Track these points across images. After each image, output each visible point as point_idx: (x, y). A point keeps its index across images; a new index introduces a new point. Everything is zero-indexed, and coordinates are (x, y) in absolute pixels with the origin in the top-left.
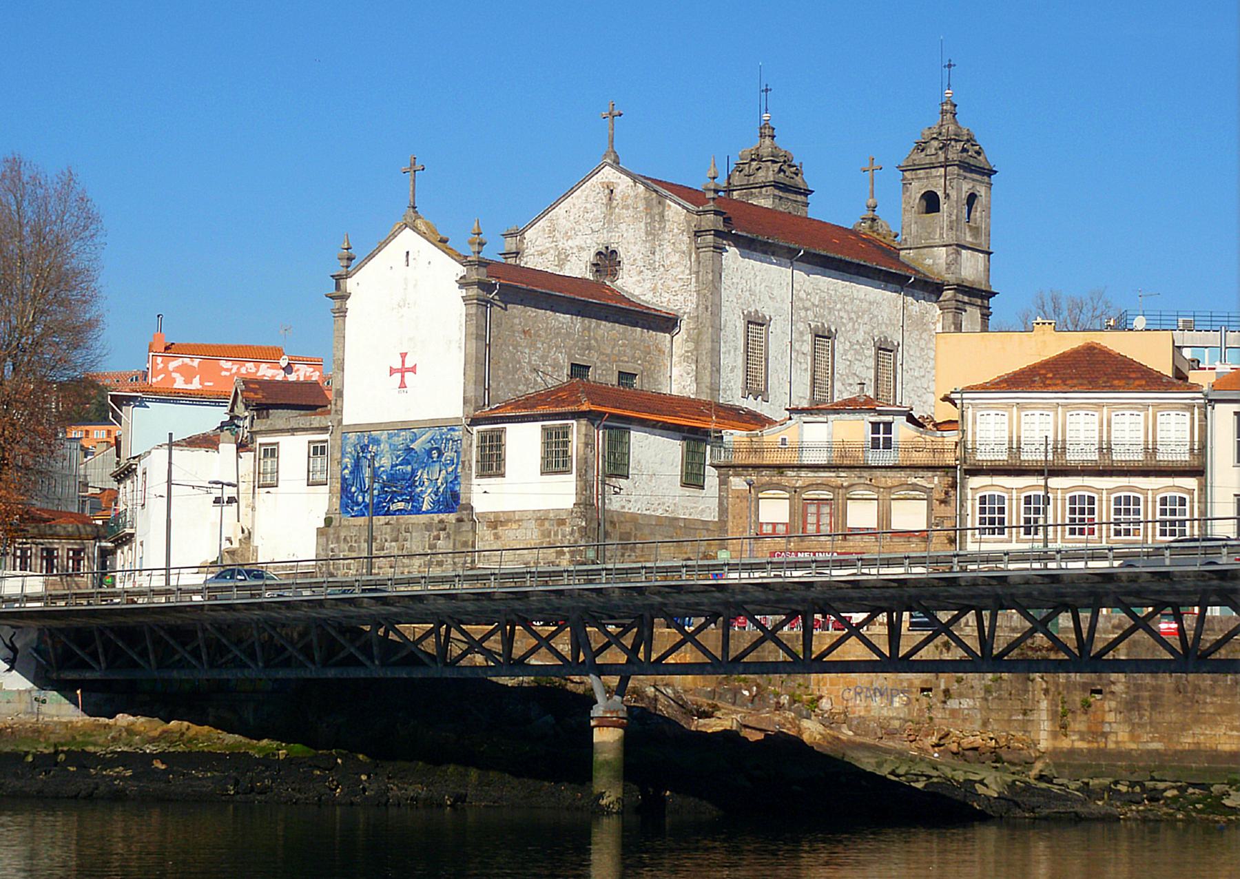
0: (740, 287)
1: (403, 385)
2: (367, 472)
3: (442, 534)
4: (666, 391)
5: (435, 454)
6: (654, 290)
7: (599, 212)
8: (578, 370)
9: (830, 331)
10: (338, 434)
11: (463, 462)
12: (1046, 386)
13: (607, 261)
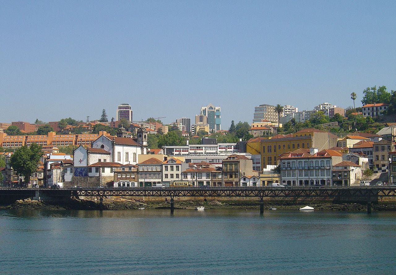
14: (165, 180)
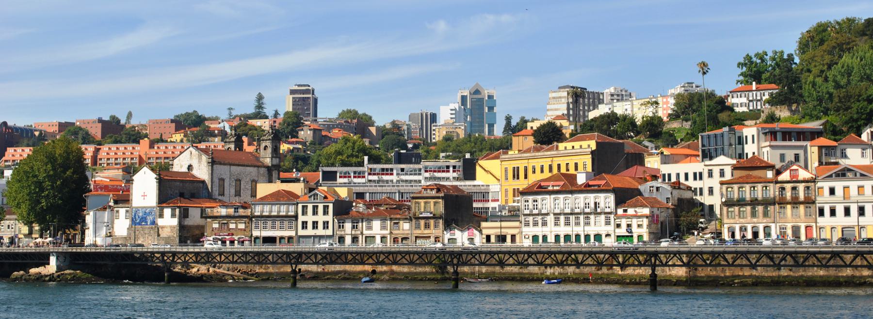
13: (190, 167)
14: (301, 232)
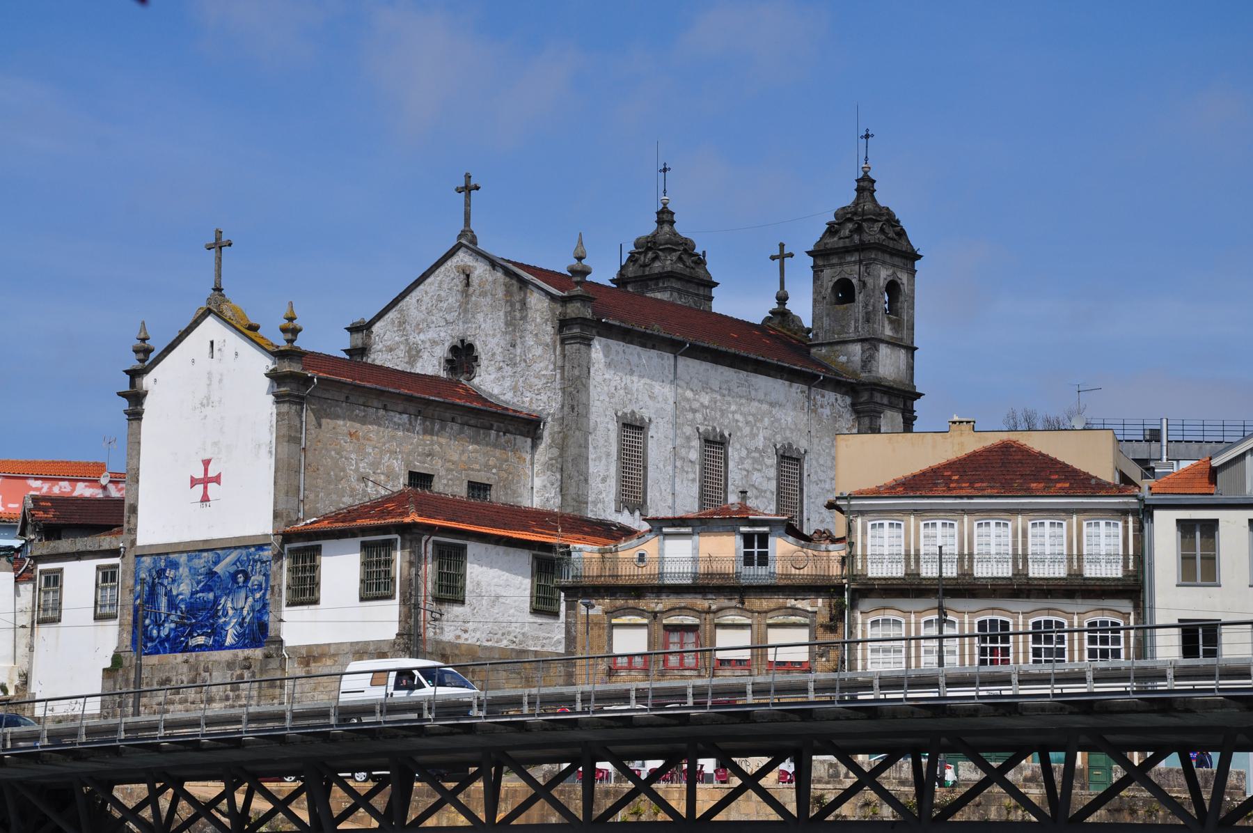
0: (613, 384)
1: (205, 499)
2: (163, 602)
3: (247, 675)
4: (526, 503)
5: (241, 578)
6: (515, 389)
7: (453, 300)
8: (419, 480)
9: (722, 436)
10: (130, 557)
11: (273, 587)
12: (950, 489)
13: (463, 357)
